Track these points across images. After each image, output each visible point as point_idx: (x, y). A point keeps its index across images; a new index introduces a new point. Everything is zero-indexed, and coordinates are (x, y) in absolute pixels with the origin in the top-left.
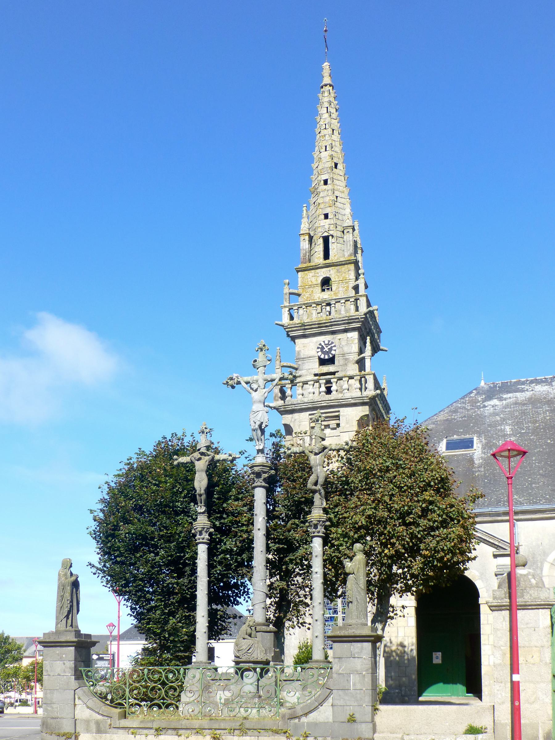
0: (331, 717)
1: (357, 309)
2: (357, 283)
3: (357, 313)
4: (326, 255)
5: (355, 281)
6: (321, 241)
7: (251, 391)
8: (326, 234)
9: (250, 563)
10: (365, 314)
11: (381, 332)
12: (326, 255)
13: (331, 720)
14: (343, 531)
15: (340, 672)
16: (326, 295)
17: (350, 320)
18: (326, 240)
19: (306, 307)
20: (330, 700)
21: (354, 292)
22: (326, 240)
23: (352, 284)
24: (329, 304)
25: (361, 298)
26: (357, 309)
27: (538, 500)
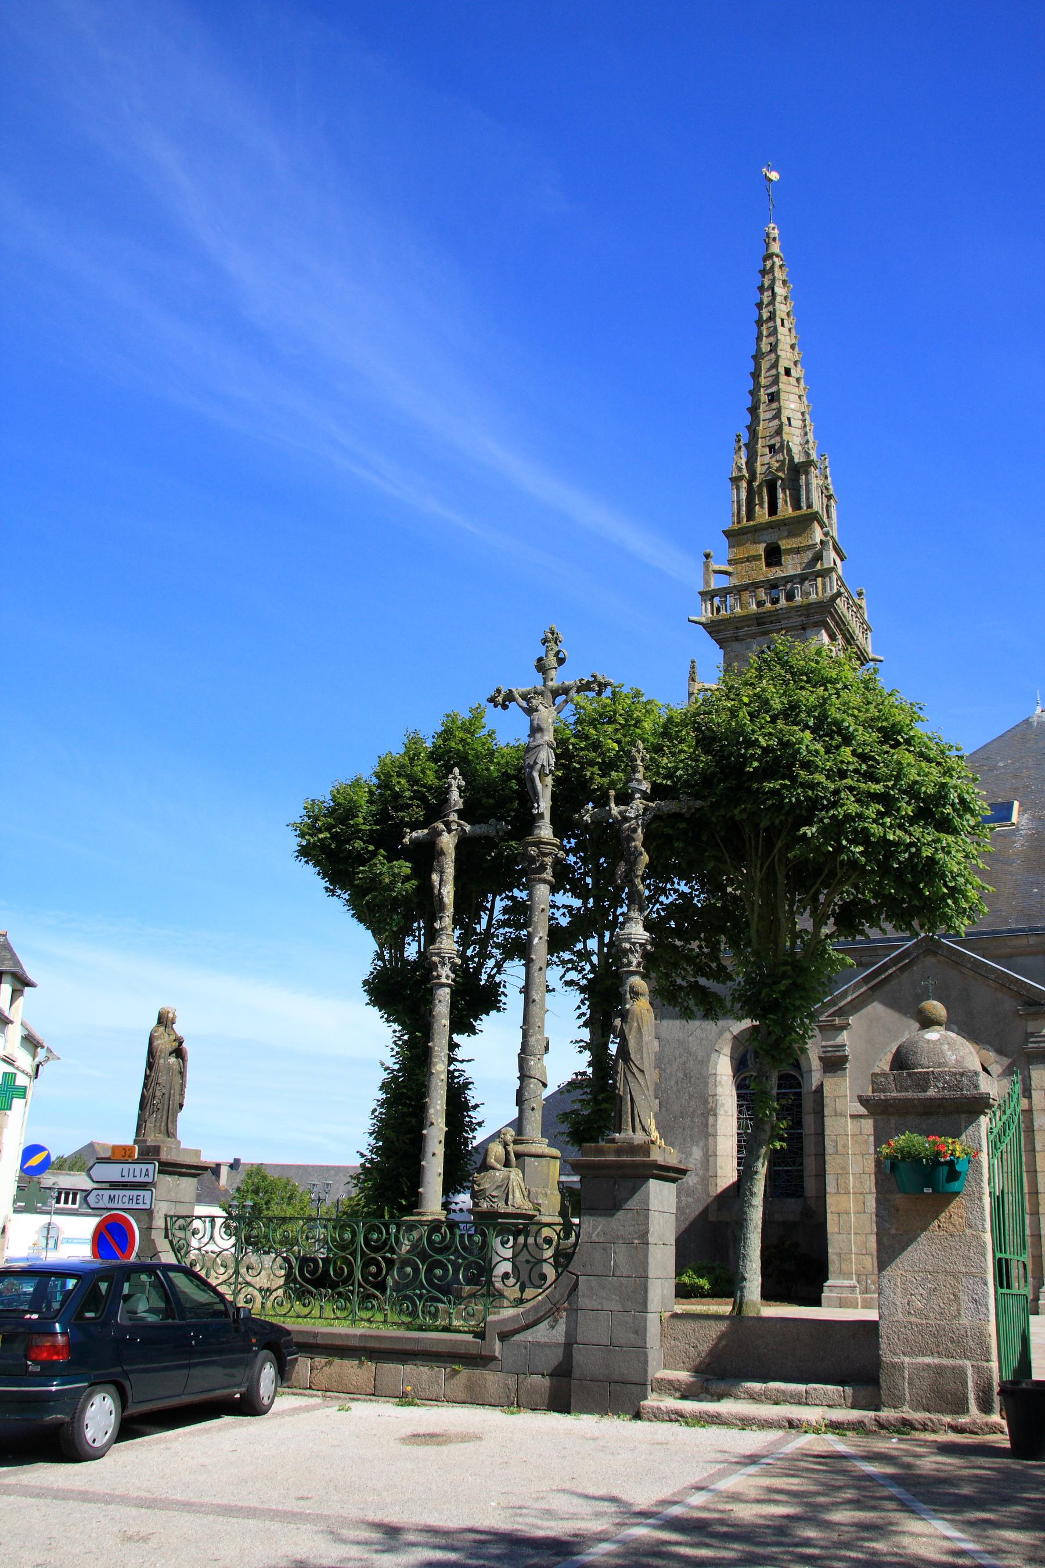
4: (773, 510)
12: (773, 510)
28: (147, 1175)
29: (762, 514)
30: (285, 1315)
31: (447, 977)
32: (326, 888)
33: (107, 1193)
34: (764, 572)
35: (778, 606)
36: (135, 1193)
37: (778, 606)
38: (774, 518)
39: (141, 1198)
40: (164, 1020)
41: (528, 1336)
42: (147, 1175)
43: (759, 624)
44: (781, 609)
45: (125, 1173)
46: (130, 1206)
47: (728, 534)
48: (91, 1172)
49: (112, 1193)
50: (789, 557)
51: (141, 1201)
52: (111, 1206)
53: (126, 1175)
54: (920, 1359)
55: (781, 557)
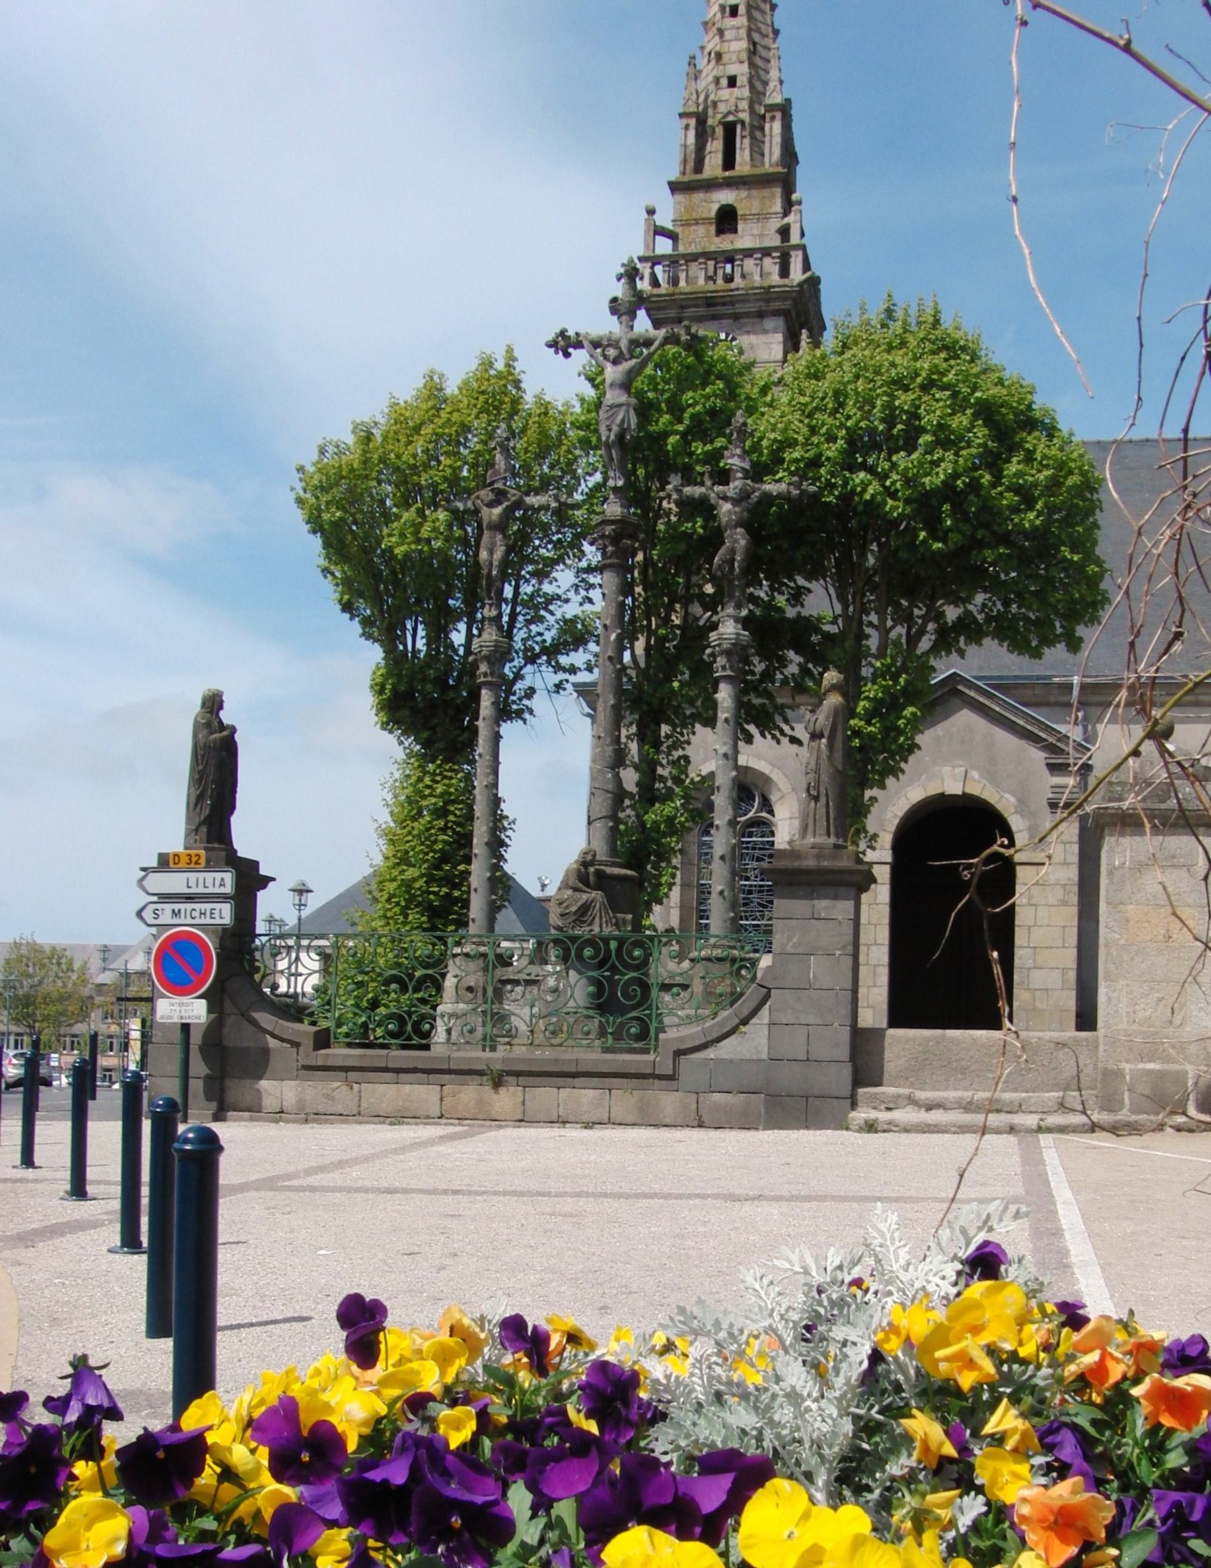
0: (766, 1050)
1: (784, 272)
2: (786, 220)
3: (786, 281)
4: (729, 161)
5: (783, 218)
6: (720, 131)
7: (993, 1510)
8: (731, 118)
9: (56, 1512)
10: (800, 285)
11: (221, 1149)
12: (729, 161)
13: (764, 1056)
14: (886, 690)
15: (789, 949)
16: (725, 243)
17: (767, 294)
18: (730, 130)
19: (687, 261)
20: (765, 1011)
21: (779, 237)
22: (730, 130)
23: (776, 224)
24: (731, 260)
25: (793, 253)
26: (784, 272)
27: (1035, 577)
28: (222, 885)
29: (713, 165)
30: (561, 1045)
31: (724, 668)
32: (1101, 511)
33: (169, 908)
34: (703, 238)
35: (733, 285)
36: (208, 906)
37: (733, 285)
38: (699, 177)
39: (217, 913)
40: (213, 703)
41: (710, 1053)
42: (222, 885)
43: (709, 305)
44: (737, 289)
45: (192, 883)
46: (203, 921)
47: (670, 183)
48: (144, 883)
49: (176, 907)
50: (750, 225)
51: (217, 915)
52: (176, 921)
53: (211, 886)
54: (1141, 1066)
55: (736, 224)
